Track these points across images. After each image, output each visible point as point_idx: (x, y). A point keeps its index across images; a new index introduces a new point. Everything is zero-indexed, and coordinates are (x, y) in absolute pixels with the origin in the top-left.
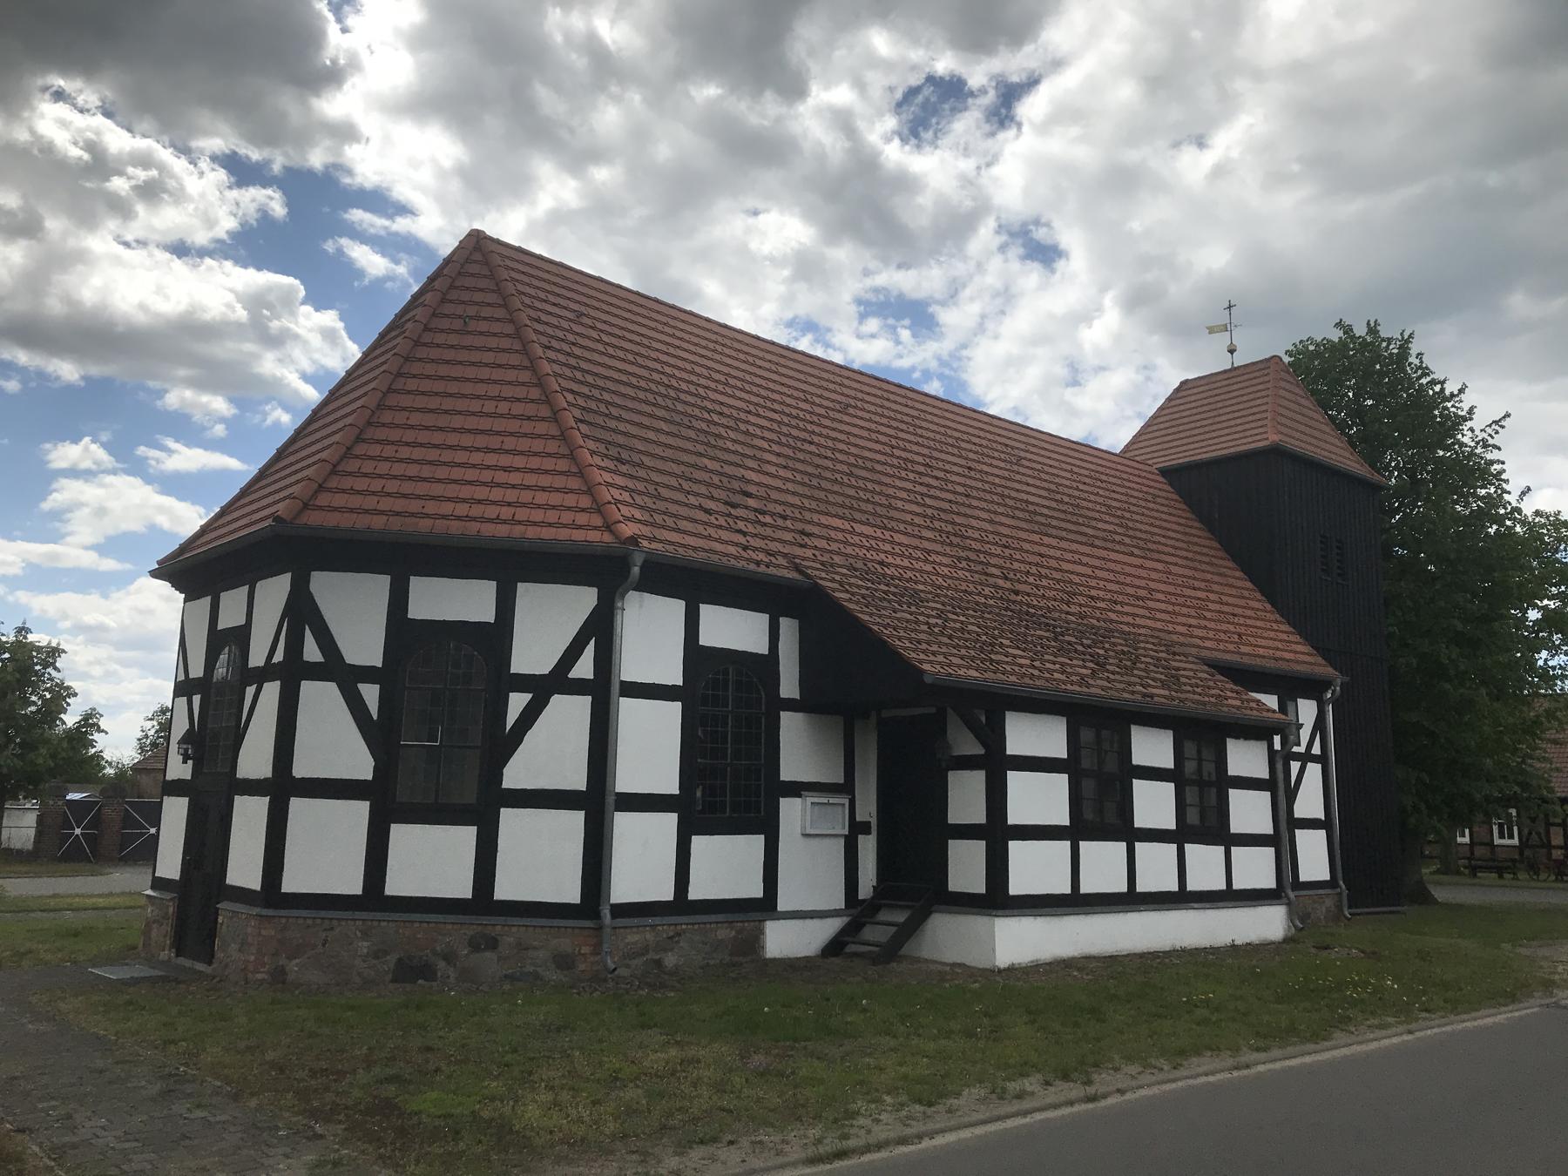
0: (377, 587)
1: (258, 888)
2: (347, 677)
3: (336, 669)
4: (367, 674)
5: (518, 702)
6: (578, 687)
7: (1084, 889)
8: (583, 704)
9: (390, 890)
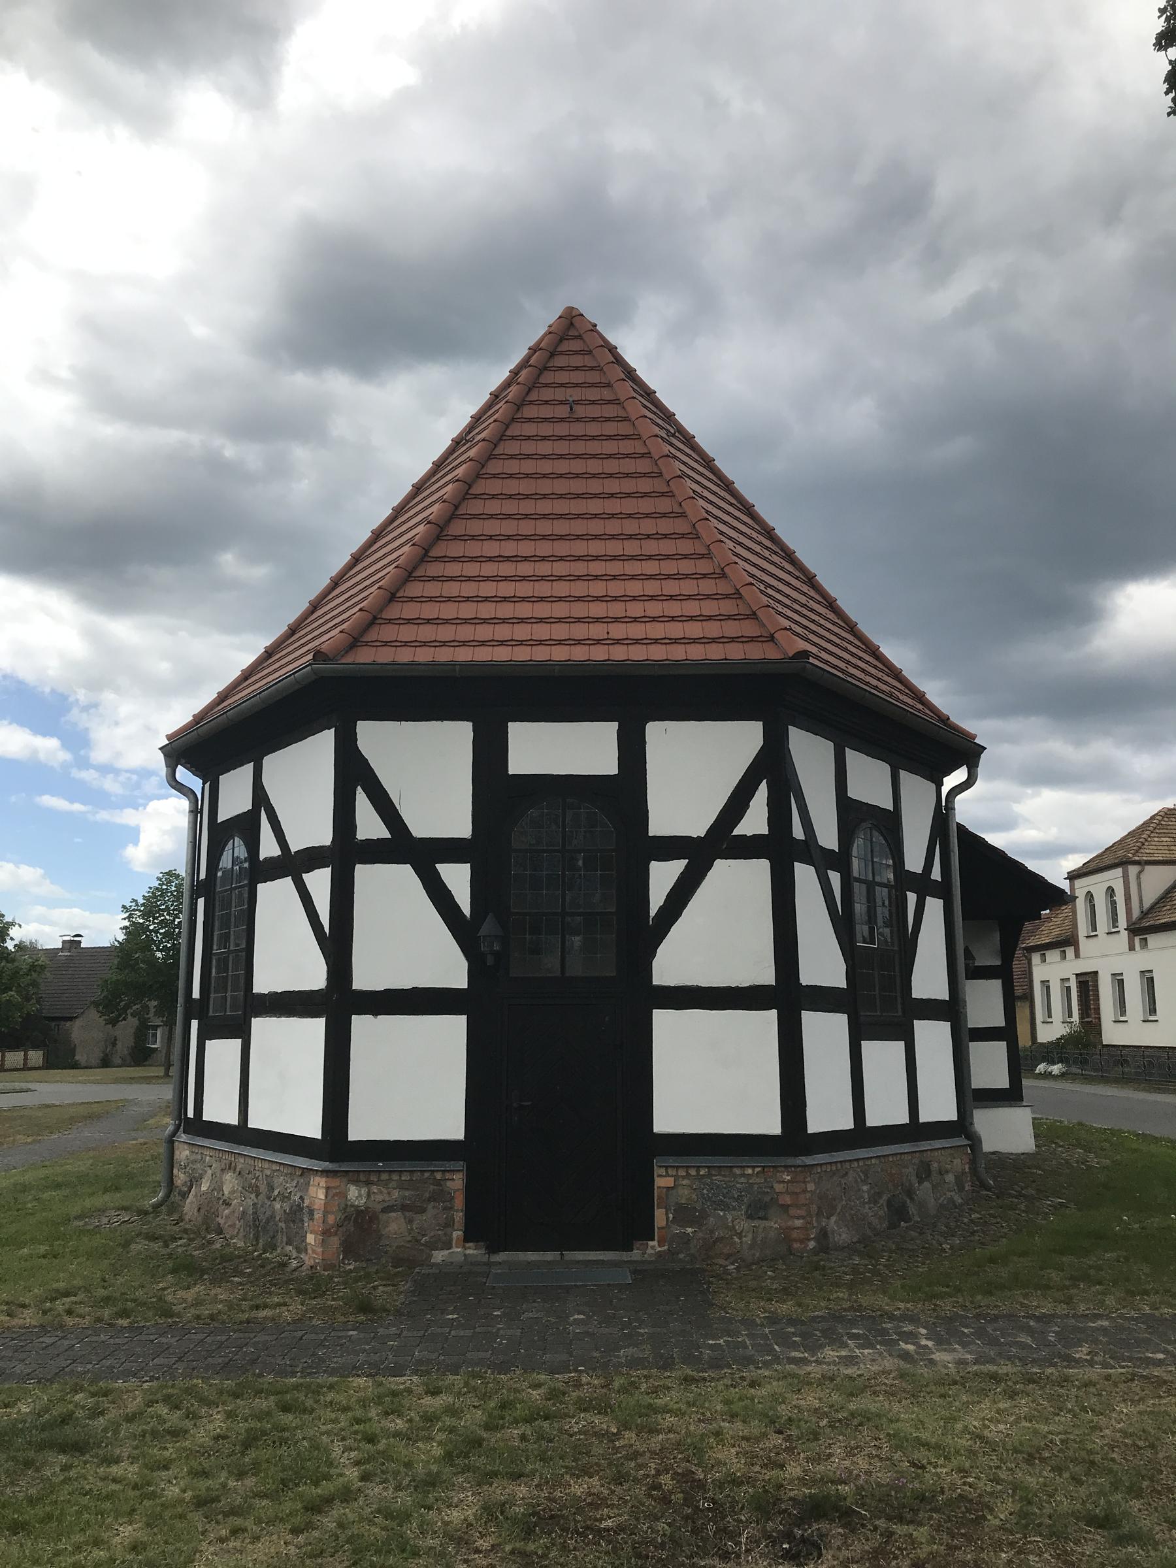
0: (454, 740)
1: (318, 1135)
2: (424, 856)
3: (402, 847)
4: (450, 850)
5: (663, 876)
6: (747, 848)
7: (872, 1121)
8: (760, 870)
9: (354, 1135)
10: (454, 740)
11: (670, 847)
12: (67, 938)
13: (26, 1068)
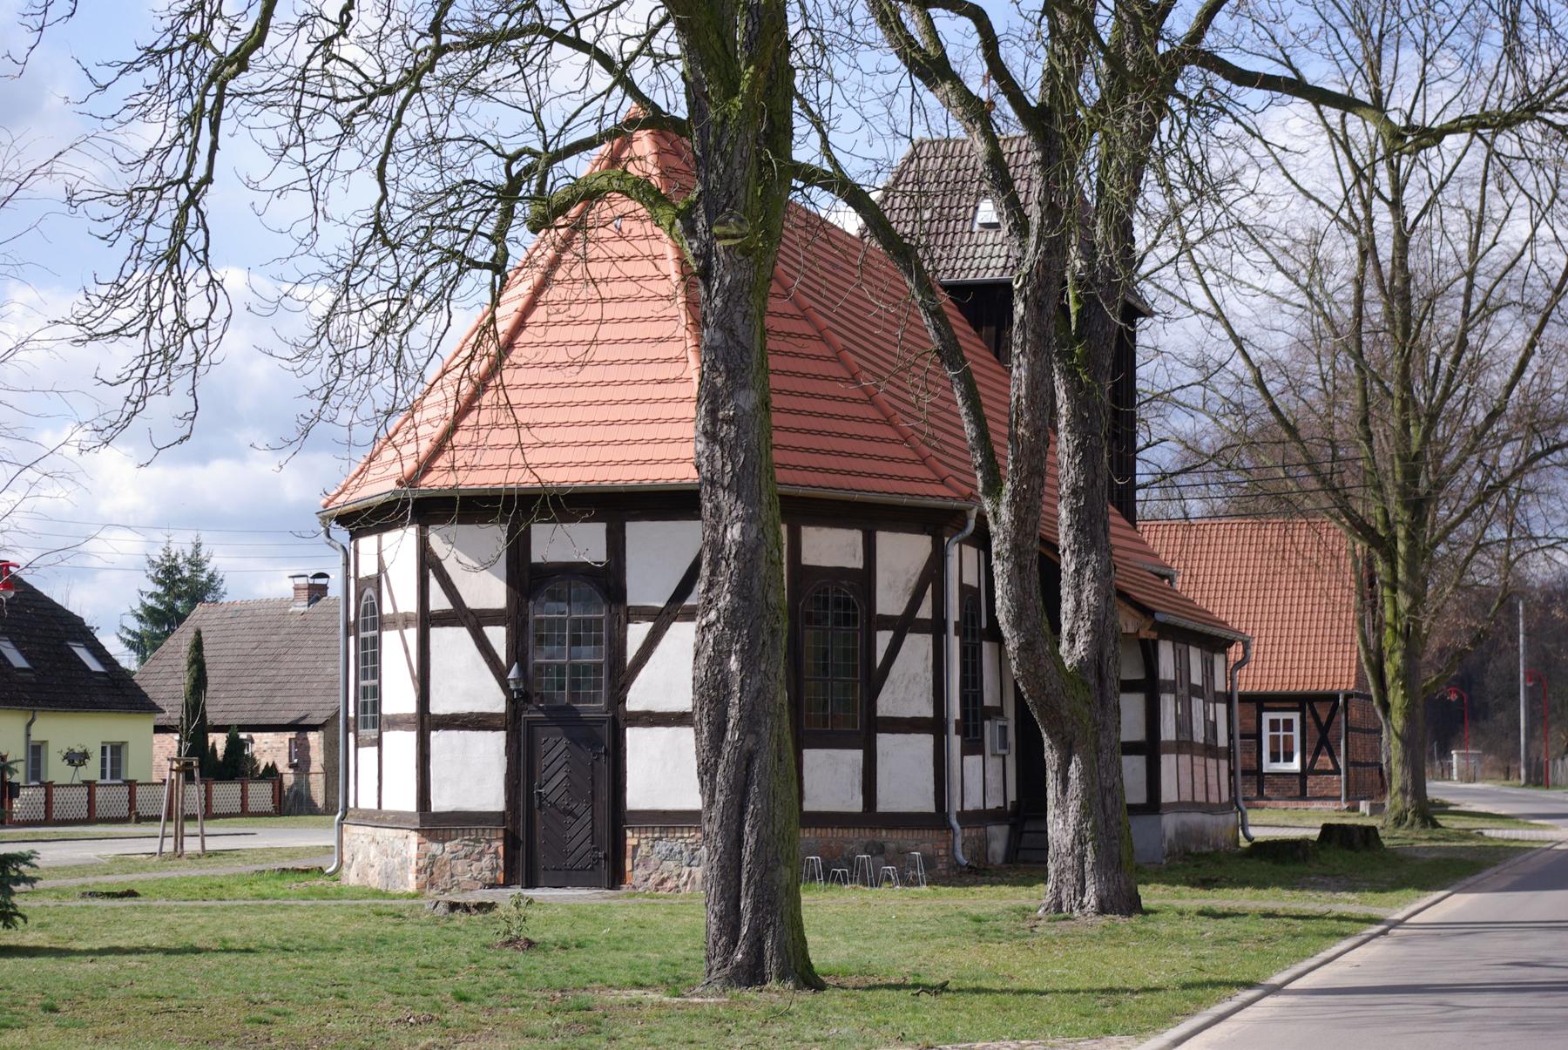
0: (494, 536)
2: (475, 621)
4: (493, 617)
10: (494, 536)
11: (643, 613)
12: (302, 581)
13: (244, 812)
